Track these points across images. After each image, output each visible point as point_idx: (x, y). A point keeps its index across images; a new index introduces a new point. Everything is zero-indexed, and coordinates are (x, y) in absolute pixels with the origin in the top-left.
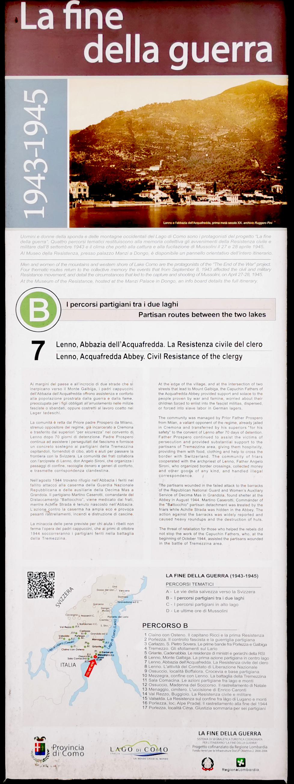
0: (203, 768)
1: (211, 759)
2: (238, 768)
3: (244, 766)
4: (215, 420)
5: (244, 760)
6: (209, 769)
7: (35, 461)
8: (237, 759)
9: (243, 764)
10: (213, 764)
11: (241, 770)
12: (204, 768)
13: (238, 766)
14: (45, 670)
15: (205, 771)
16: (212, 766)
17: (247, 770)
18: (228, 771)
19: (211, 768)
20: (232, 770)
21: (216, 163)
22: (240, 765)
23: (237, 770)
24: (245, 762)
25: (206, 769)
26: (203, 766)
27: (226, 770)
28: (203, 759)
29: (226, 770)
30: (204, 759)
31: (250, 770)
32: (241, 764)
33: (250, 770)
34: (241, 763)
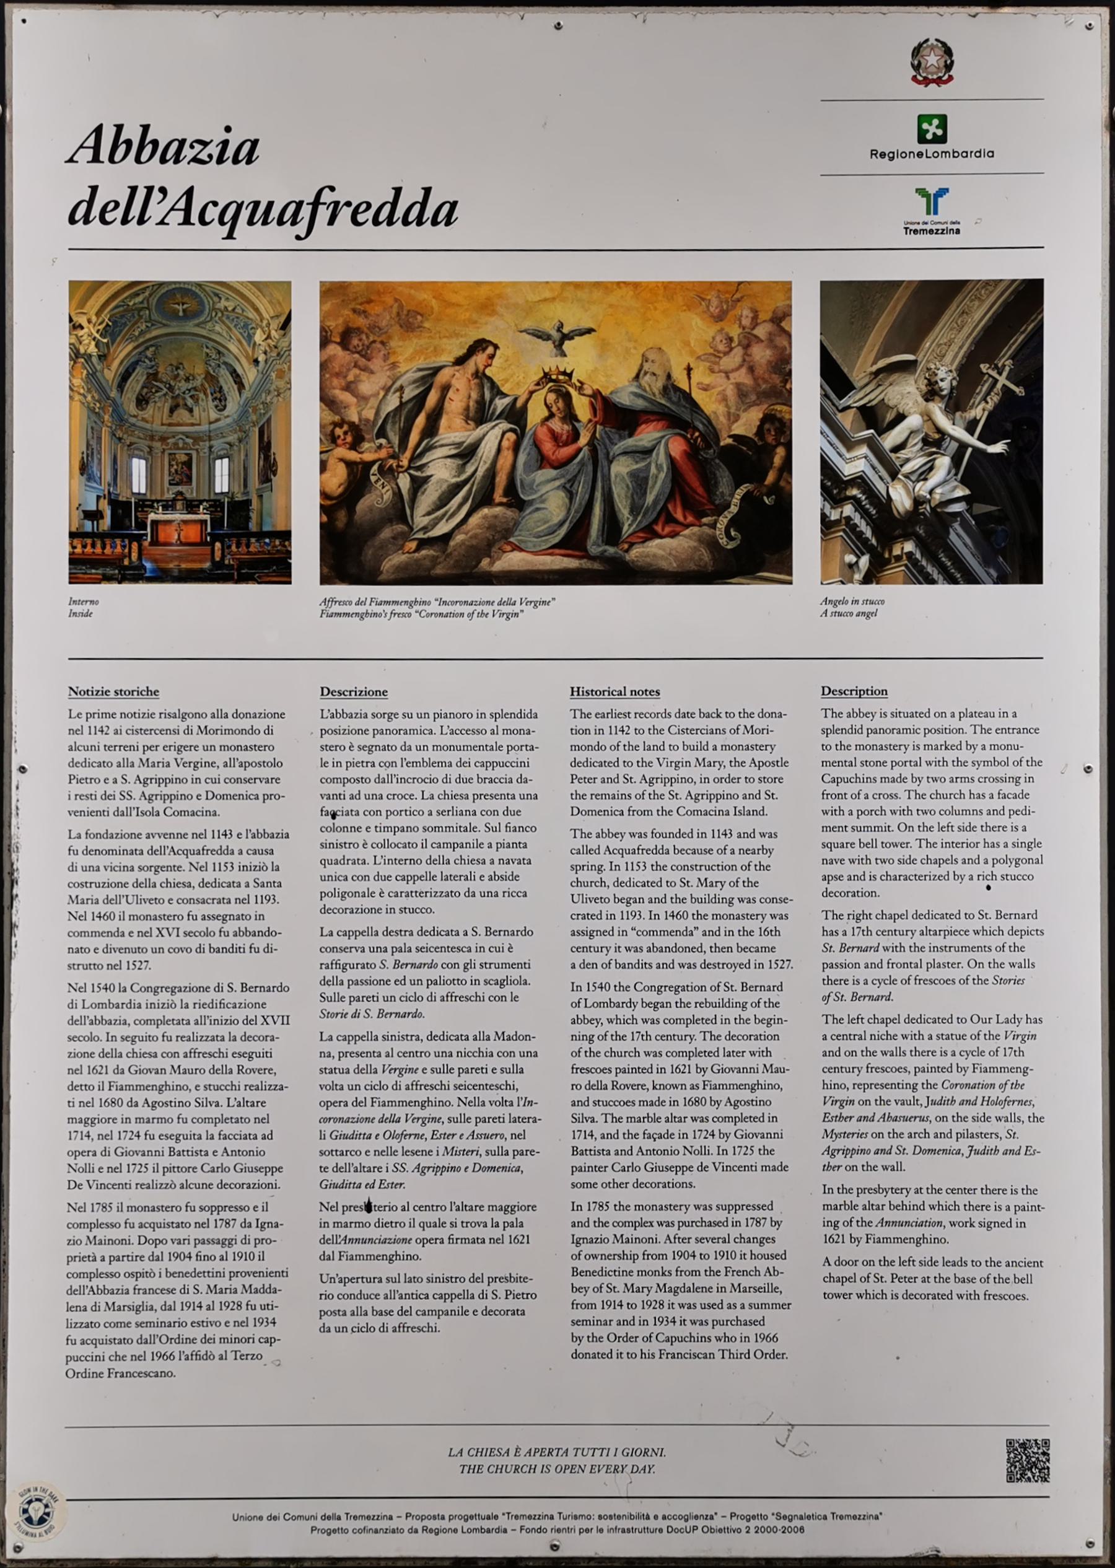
0: (914, 79)
1: (944, 44)
2: (923, 147)
3: (942, 139)
4: (736, 721)
5: (943, 120)
6: (939, 81)
7: (586, 731)
8: (920, 117)
9: (940, 132)
10: (952, 62)
11: (936, 154)
12: (920, 78)
13: (922, 139)
14: (401, 402)
15: (922, 86)
16: (949, 67)
17: (955, 154)
18: (892, 159)
19: (946, 77)
20: (904, 155)
21: (497, 546)
22: (929, 136)
23: (920, 155)
24: (944, 128)
25: (926, 82)
26: (917, 68)
27: (883, 155)
28: (916, 44)
29: (883, 155)
30: (920, 45)
31: (966, 154)
32: (22, 770)
33: (966, 154)
34: (932, 129)
